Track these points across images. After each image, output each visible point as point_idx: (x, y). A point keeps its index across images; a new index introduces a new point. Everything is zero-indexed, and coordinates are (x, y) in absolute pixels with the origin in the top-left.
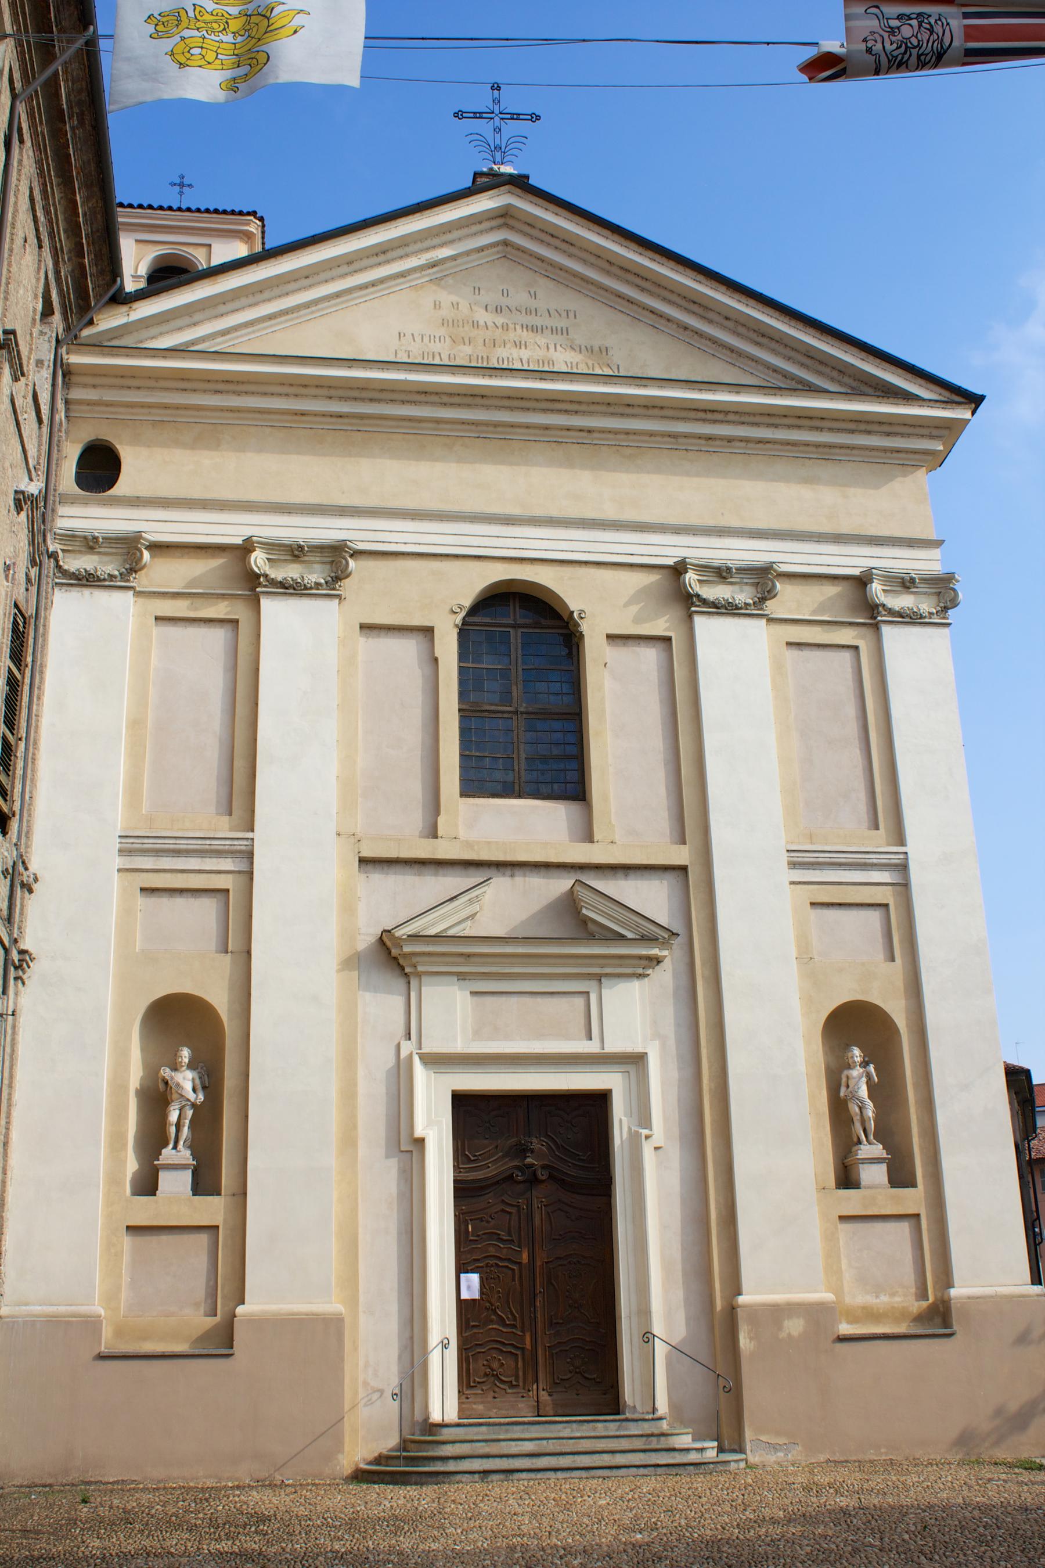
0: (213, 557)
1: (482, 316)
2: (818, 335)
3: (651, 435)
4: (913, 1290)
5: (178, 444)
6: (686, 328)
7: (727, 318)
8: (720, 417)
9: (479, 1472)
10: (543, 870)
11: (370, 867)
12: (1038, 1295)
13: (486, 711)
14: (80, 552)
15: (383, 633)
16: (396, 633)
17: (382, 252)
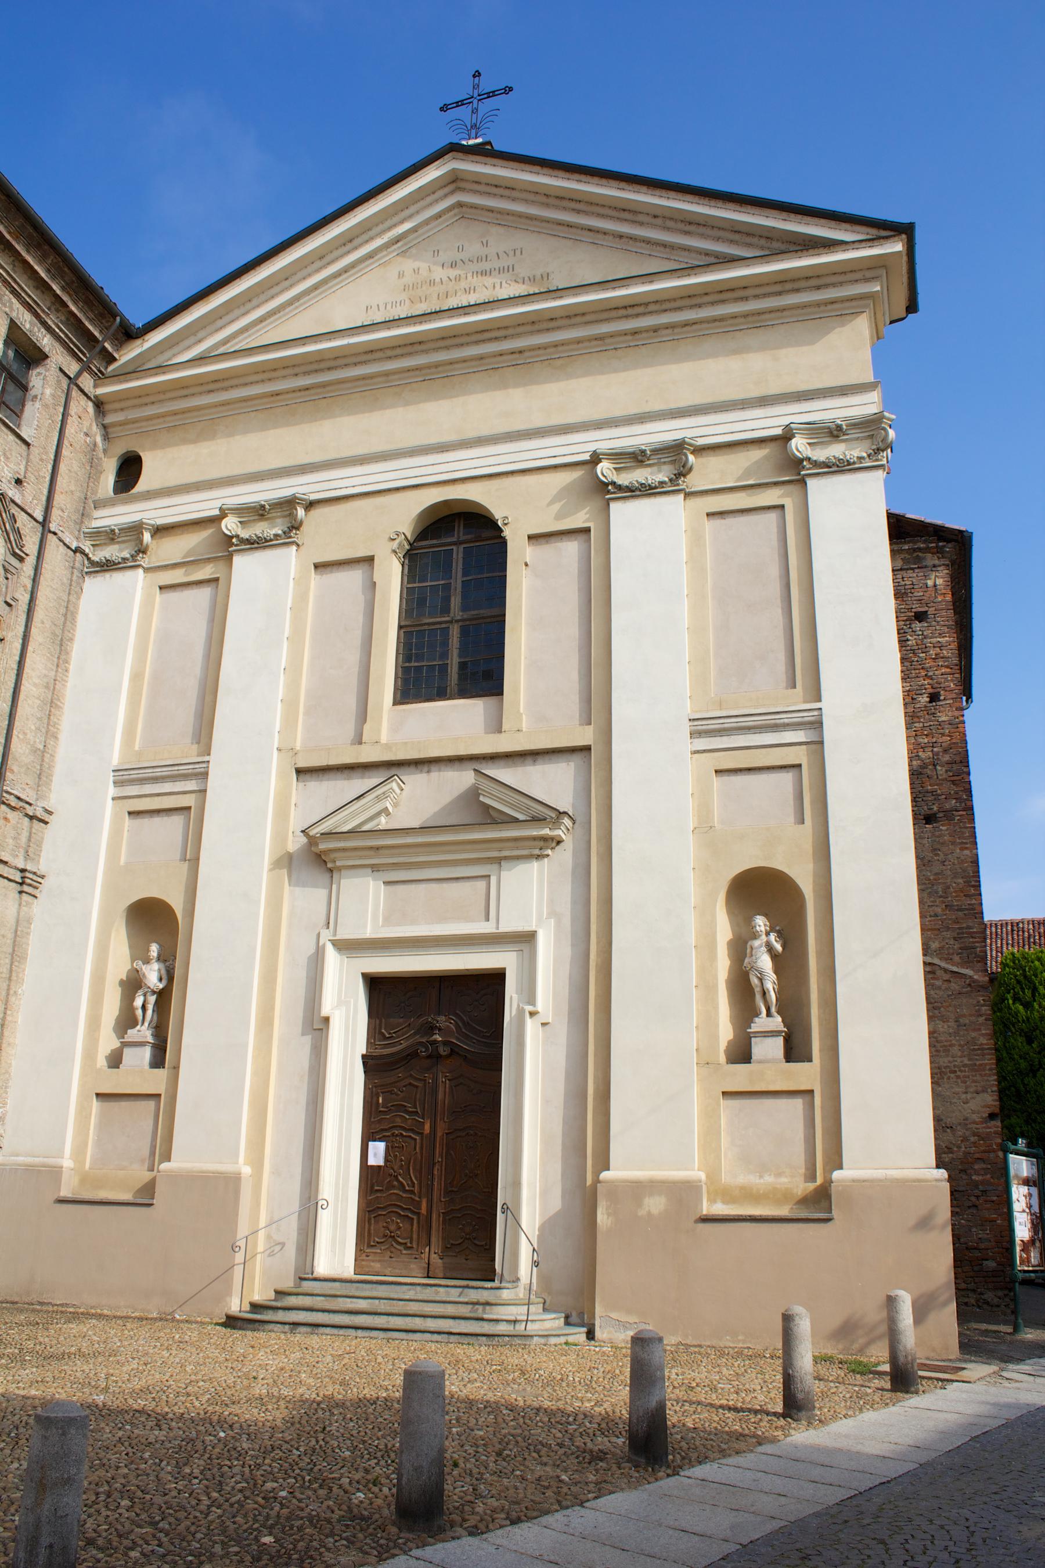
0: (205, 529)
1: (439, 273)
2: (738, 207)
3: (578, 343)
4: (803, 1171)
5: (185, 441)
6: (621, 237)
7: (655, 217)
8: (641, 310)
9: (290, 1324)
10: (457, 764)
11: (308, 776)
12: (937, 1180)
13: (425, 624)
14: (105, 544)
15: (335, 568)
16: (346, 567)
17: (348, 241)
